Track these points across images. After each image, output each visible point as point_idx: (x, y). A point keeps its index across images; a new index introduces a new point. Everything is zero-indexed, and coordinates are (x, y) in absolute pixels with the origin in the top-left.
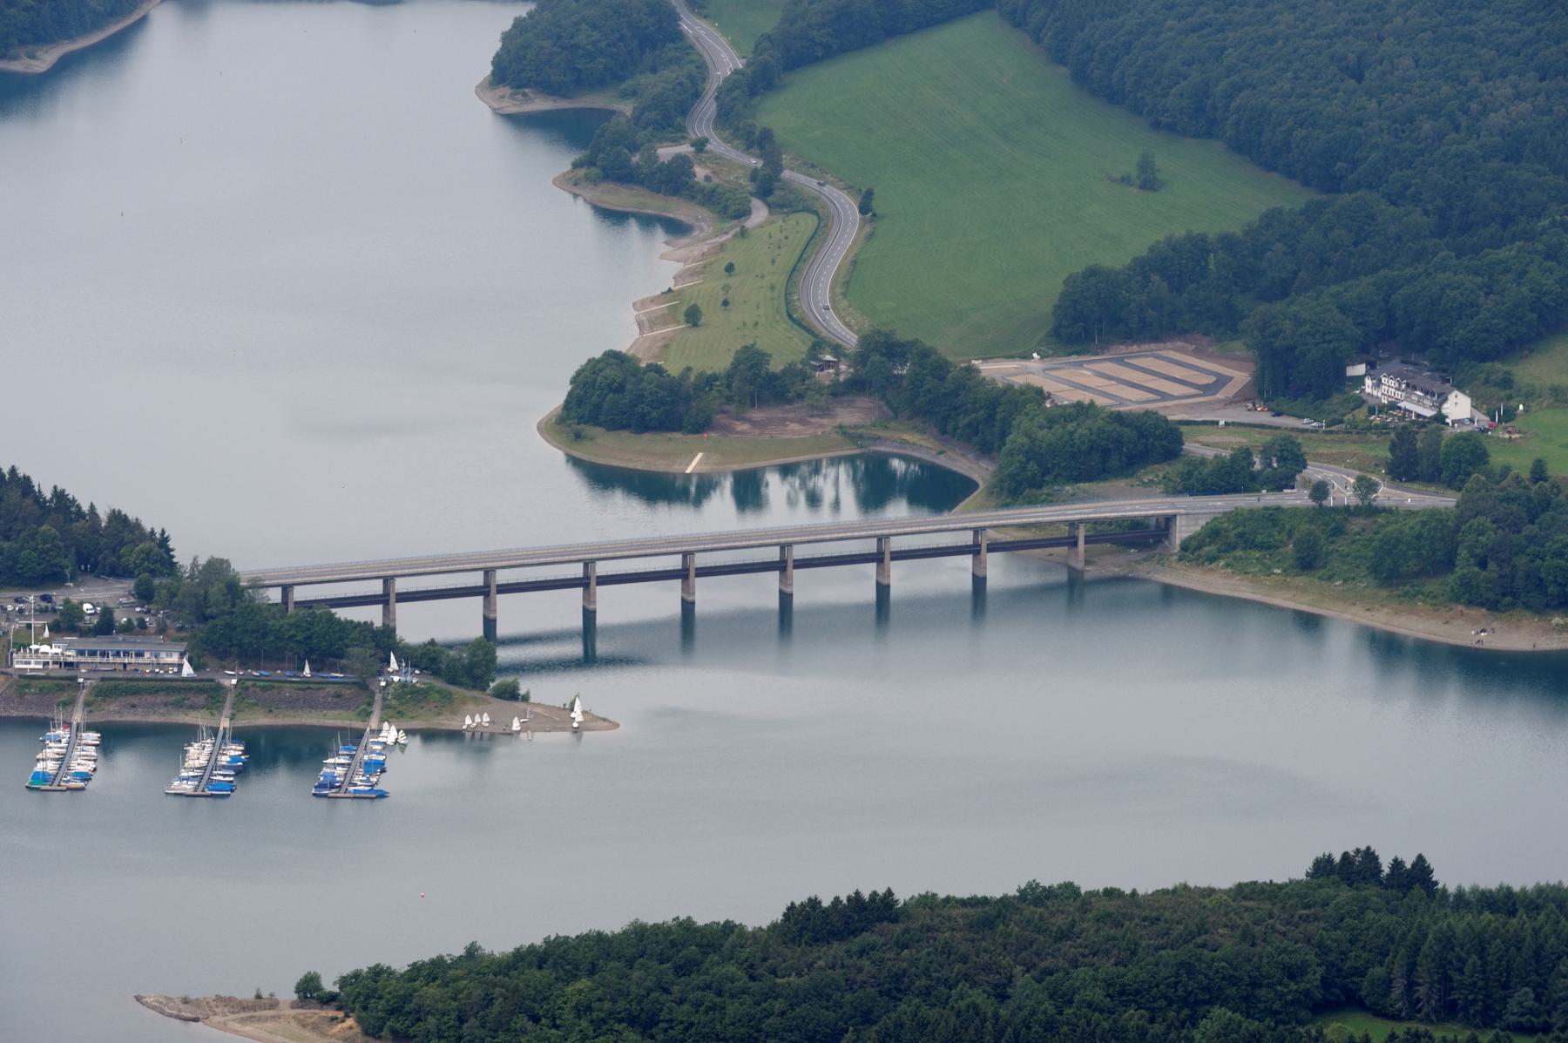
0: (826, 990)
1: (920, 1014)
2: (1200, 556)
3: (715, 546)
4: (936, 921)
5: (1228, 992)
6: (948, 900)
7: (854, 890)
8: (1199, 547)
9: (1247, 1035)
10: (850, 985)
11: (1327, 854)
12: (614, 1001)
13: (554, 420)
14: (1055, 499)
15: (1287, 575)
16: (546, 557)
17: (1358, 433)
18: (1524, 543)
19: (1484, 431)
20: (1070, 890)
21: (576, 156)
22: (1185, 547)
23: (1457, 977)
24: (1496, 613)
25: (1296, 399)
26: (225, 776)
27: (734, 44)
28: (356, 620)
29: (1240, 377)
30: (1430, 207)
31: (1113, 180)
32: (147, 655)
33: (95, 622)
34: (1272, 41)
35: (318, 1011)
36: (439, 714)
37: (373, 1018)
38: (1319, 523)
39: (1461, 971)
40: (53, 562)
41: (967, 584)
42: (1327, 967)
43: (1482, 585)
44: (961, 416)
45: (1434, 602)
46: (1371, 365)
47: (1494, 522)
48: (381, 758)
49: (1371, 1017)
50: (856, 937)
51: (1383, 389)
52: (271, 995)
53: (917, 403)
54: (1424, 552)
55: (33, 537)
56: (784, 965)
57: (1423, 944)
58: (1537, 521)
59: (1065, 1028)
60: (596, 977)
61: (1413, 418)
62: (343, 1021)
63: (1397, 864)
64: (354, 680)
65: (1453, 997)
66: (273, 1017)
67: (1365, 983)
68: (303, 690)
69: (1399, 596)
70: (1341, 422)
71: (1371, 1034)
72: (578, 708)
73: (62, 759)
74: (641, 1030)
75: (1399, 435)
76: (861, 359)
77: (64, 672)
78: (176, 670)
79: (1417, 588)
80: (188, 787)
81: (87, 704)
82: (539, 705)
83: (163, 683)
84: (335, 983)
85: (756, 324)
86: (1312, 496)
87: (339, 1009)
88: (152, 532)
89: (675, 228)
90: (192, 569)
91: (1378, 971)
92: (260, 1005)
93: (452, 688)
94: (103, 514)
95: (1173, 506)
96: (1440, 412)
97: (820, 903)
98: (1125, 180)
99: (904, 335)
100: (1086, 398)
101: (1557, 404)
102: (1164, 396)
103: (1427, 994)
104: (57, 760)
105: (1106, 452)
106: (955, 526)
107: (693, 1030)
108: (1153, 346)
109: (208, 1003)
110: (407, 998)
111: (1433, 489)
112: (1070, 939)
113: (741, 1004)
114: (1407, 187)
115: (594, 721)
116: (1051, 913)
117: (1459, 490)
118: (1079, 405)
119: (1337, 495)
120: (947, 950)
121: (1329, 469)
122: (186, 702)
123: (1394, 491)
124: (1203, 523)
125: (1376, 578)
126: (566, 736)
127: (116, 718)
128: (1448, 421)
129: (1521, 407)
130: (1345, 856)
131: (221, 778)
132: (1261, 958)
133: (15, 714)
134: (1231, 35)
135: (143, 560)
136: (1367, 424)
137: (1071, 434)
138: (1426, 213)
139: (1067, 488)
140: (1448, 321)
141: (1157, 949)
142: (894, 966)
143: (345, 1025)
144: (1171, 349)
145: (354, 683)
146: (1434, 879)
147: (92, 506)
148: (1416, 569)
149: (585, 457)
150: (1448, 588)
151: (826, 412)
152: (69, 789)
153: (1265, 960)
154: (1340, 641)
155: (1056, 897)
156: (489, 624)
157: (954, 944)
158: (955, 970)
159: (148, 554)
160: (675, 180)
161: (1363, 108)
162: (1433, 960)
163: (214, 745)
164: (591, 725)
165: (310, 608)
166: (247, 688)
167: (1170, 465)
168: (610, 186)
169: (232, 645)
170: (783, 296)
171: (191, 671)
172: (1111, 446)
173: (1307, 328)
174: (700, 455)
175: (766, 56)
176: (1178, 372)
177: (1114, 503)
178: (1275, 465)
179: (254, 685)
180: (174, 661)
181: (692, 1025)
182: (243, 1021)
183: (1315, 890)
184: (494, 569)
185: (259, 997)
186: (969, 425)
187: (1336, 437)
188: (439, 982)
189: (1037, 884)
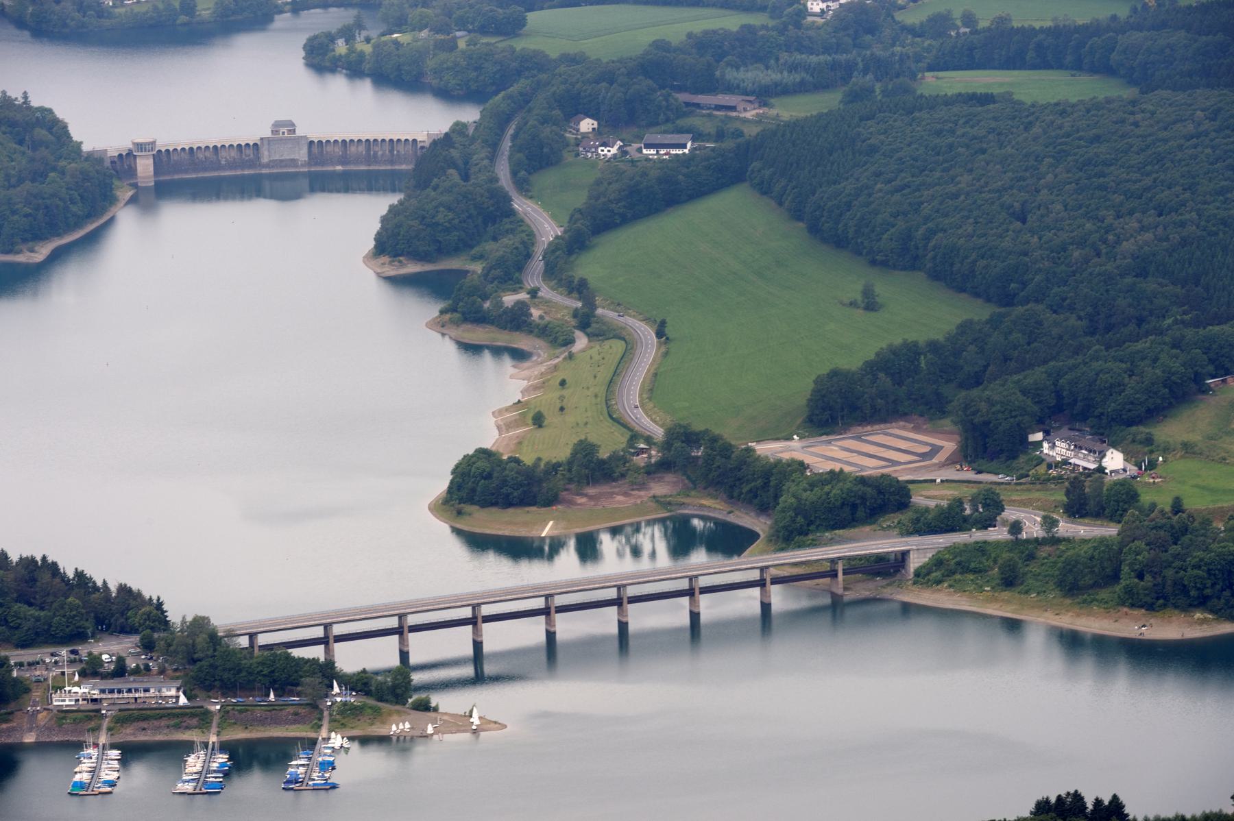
2: (929, 580)
8: (928, 574)
15: (995, 592)
18: (1171, 559)
19: (1134, 478)
21: (441, 305)
22: (918, 574)
25: (992, 460)
26: (216, 778)
28: (306, 657)
29: (949, 446)
30: (1082, 314)
32: (152, 691)
33: (112, 667)
34: (956, 196)
36: (372, 724)
38: (1017, 551)
40: (78, 624)
41: (757, 609)
46: (1047, 433)
47: (1147, 544)
48: (332, 759)
51: (1057, 450)
53: (710, 476)
54: (1096, 570)
61: (1081, 470)
63: (1098, 802)
64: (308, 702)
69: (1079, 603)
70: (1027, 476)
72: (475, 714)
73: (94, 771)
75: (1071, 483)
76: (667, 445)
77: (91, 706)
78: (174, 700)
80: (189, 788)
81: (109, 729)
83: (166, 711)
85: (586, 424)
86: (1010, 532)
88: (151, 599)
89: (519, 355)
90: (182, 624)
93: (380, 704)
94: (113, 587)
95: (907, 544)
96: (1100, 465)
98: (853, 304)
99: (698, 426)
100: (837, 467)
101: (1187, 455)
104: (90, 772)
105: (854, 507)
108: (882, 426)
111: (1099, 522)
114: (1064, 300)
115: (486, 724)
117: (1120, 522)
118: (832, 472)
119: (1028, 530)
121: (1017, 511)
124: (930, 555)
125: (1061, 591)
126: (466, 736)
127: (132, 738)
128: (1107, 471)
129: (1161, 459)
130: (1059, 798)
131: (214, 779)
133: (55, 739)
134: (926, 193)
135: (145, 619)
136: (1047, 476)
137: (828, 494)
138: (1080, 318)
139: (827, 534)
144: (897, 428)
145: (307, 704)
146: (1126, 812)
147: (105, 582)
148: (1091, 582)
149: (466, 528)
151: (642, 486)
152: (100, 793)
154: (1035, 639)
156: (404, 656)
160: (517, 320)
163: (206, 755)
164: (485, 727)
165: (272, 649)
166: (228, 712)
167: (902, 513)
169: (216, 680)
172: (858, 502)
173: (998, 407)
174: (551, 523)
175: (578, 225)
176: (903, 445)
178: (981, 510)
179: (233, 709)
180: (173, 694)
186: (750, 491)
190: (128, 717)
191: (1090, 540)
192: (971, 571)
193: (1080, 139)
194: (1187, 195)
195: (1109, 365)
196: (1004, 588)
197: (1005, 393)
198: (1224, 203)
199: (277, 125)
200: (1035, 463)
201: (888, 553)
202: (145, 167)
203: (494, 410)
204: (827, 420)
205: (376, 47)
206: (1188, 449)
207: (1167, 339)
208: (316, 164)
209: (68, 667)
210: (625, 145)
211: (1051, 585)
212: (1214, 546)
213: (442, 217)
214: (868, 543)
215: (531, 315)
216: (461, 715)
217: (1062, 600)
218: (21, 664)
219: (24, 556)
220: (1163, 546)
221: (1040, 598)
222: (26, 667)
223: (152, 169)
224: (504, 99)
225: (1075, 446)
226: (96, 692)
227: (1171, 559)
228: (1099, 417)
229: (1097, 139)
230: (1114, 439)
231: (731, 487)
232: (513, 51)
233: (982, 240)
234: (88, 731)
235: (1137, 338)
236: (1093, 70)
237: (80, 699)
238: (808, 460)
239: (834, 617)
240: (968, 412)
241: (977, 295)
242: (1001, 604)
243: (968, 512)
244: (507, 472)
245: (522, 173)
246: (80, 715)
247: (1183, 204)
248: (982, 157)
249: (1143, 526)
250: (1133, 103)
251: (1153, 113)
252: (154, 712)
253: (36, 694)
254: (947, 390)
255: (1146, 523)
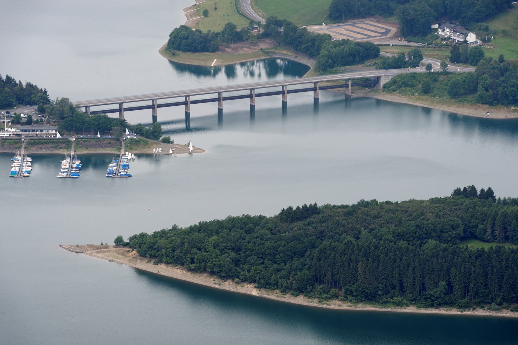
0: (299, 237)
1: (332, 245)
2: (390, 90)
3: (229, 90)
4: (333, 213)
5: (433, 235)
6: (334, 206)
7: (304, 204)
8: (389, 87)
9: (443, 249)
10: (306, 235)
11: (458, 188)
12: (226, 243)
13: (164, 49)
14: (338, 72)
15: (420, 95)
16: (173, 95)
17: (438, 47)
18: (501, 83)
19: (481, 46)
20: (374, 202)
22: (384, 87)
23: (509, 227)
24: (492, 106)
25: (415, 36)
26: (76, 171)
28: (114, 118)
29: (394, 30)
32: (44, 131)
33: (26, 120)
35: (123, 249)
36: (144, 149)
37: (143, 250)
38: (429, 78)
39: (510, 226)
40: (9, 100)
41: (312, 101)
42: (465, 225)
43: (487, 97)
44: (303, 45)
45: (471, 103)
46: (440, 25)
47: (490, 76)
48: (127, 164)
49: (480, 242)
50: (306, 219)
51: (445, 32)
52: (106, 244)
54: (466, 87)
56: (283, 229)
57: (497, 217)
58: (504, 75)
60: (219, 235)
61: (457, 42)
62: (132, 252)
63: (482, 190)
64: (115, 138)
65: (508, 234)
66: (108, 251)
67: (478, 230)
68: (97, 141)
69: (459, 101)
70: (432, 44)
71: (484, 246)
72: (191, 145)
73: (20, 166)
74: (235, 252)
75: (453, 48)
76: (267, 26)
77: (17, 137)
78: (54, 136)
79: (464, 99)
80: (64, 175)
81: (25, 148)
83: (51, 140)
84: (128, 239)
85: (228, 15)
86: (427, 69)
87: (130, 248)
88: (41, 90)
90: (56, 101)
91: (481, 226)
92: (102, 247)
94: (24, 84)
96: (465, 40)
97: (292, 208)
99: (281, 18)
100: (346, 38)
101: (504, 36)
102: (370, 37)
103: (499, 234)
104: (19, 167)
105: (354, 56)
107: (254, 252)
109: (85, 247)
110: (155, 243)
111: (466, 65)
112: (378, 218)
113: (270, 243)
115: (196, 149)
116: (371, 210)
117: (475, 65)
118: (343, 40)
119: (434, 68)
120: (338, 223)
121: (428, 59)
122: (59, 146)
123: (453, 66)
124: (390, 78)
125: (450, 96)
126: (186, 155)
127: (36, 152)
128: (468, 42)
129: (492, 37)
130: (465, 188)
131: (75, 172)
132: (443, 223)
135: (40, 99)
136: (441, 44)
137: (343, 50)
139: (342, 68)
140: (466, 9)
141: (408, 221)
142: (320, 229)
143: (132, 253)
144: (369, 21)
145: (115, 139)
146: (494, 195)
147: (20, 82)
148: (463, 92)
149: (177, 61)
151: (256, 44)
153: (445, 224)
154: (436, 117)
155: (370, 204)
156: (155, 118)
157: (340, 221)
158: (341, 229)
159: (42, 97)
162: (501, 222)
163: (70, 160)
164: (195, 151)
165: (98, 113)
167: (376, 59)
169: (73, 127)
170: (235, 6)
171: (60, 136)
172: (356, 54)
173: (419, 12)
174: (215, 60)
176: (373, 28)
177: (360, 73)
178: (413, 58)
179: (81, 140)
180: (54, 133)
181: (253, 250)
182: (98, 252)
183: (457, 200)
185: (102, 244)
186: (306, 48)
188: (164, 238)
189: (364, 200)
191: (462, 73)
192: (409, 86)
196: (424, 94)
197: (422, 6)
200: (435, 38)
201: (371, 77)
204: (338, 17)
211: (446, 93)
214: (363, 72)
216: (184, 145)
217: (450, 100)
220: (497, 77)
221: (440, 99)
225: (454, 31)
230: (470, 28)
231: (296, 45)
234: (17, 148)
237: (12, 134)
238: (332, 34)
239: (346, 105)
240: (405, 14)
242: (423, 101)
243: (407, 59)
244: (195, 36)
246: (12, 141)
249: (487, 67)
252: (45, 140)
255: (489, 66)
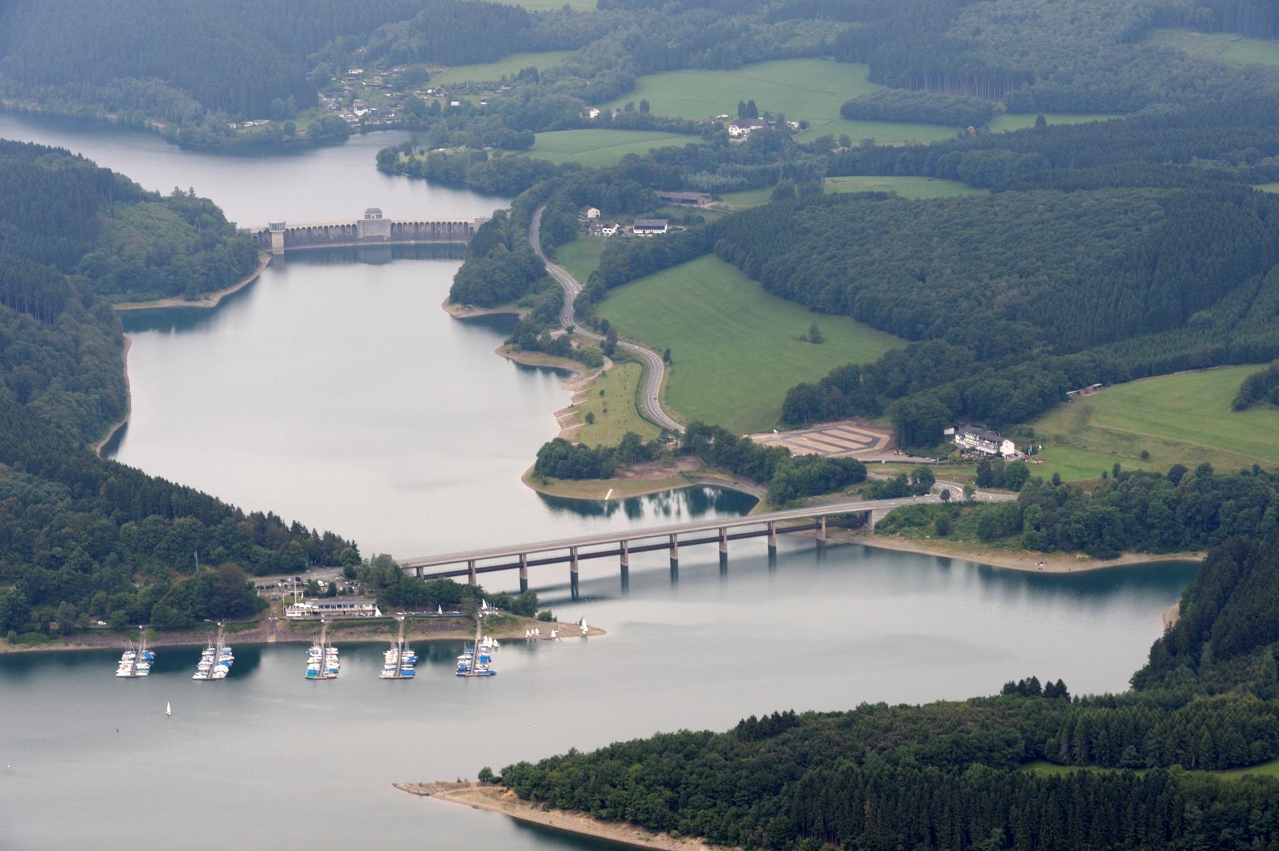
6: (820, 714)
12: (656, 775)
18: (1059, 517)
19: (1024, 460)
20: (882, 706)
21: (507, 338)
22: (877, 526)
23: (1094, 741)
25: (919, 447)
27: (575, 277)
29: (885, 438)
30: (971, 346)
31: (795, 339)
32: (356, 606)
34: (872, 263)
36: (512, 630)
39: (1096, 738)
46: (956, 429)
47: (1042, 506)
51: (967, 440)
53: (720, 458)
54: (1005, 524)
55: (287, 547)
59: (900, 778)
63: (1049, 685)
72: (584, 623)
75: (982, 464)
76: (689, 435)
77: (313, 617)
80: (391, 674)
81: (327, 633)
82: (562, 623)
87: (504, 785)
88: (348, 542)
89: (563, 374)
91: (1052, 741)
93: (517, 617)
94: (321, 535)
95: (869, 506)
98: (803, 339)
100: (813, 453)
102: (848, 449)
105: (827, 480)
106: (758, 518)
108: (835, 424)
110: (543, 778)
111: (1001, 491)
114: (957, 336)
115: (593, 631)
117: (1017, 490)
118: (810, 455)
120: (829, 740)
124: (886, 514)
126: (578, 639)
130: (1022, 682)
133: (290, 640)
134: (849, 261)
137: (809, 471)
138: (970, 349)
147: (314, 530)
150: (1020, 542)
151: (672, 465)
152: (329, 678)
154: (958, 572)
160: (561, 349)
161: (929, 296)
164: (591, 632)
166: (410, 622)
168: (527, 353)
172: (830, 476)
173: (924, 410)
174: (611, 490)
175: (597, 282)
180: (370, 609)
181: (699, 785)
184: (525, 554)
185: (459, 781)
186: (750, 468)
187: (945, 466)
190: (339, 625)
193: (957, 224)
194: (1039, 263)
195: (1000, 381)
198: (1066, 269)
199: (369, 212)
202: (277, 241)
203: (555, 411)
205: (430, 157)
206: (1059, 440)
207: (1038, 364)
208: (397, 239)
209: (298, 589)
210: (621, 227)
211: (973, 534)
212: (1089, 508)
213: (499, 276)
215: (571, 345)
218: (262, 588)
219: (255, 512)
222: (265, 590)
223: (282, 242)
224: (530, 194)
226: (316, 607)
227: (1059, 517)
228: (994, 417)
229: (970, 224)
231: (736, 466)
232: (529, 161)
233: (896, 294)
235: (1017, 364)
236: (944, 177)
239: (818, 556)
240: (902, 414)
241: (893, 332)
243: (910, 483)
244: (578, 454)
245: (551, 246)
247: (1038, 270)
248: (887, 236)
250: (991, 199)
251: (1007, 207)
253: (274, 609)
254: (880, 399)
